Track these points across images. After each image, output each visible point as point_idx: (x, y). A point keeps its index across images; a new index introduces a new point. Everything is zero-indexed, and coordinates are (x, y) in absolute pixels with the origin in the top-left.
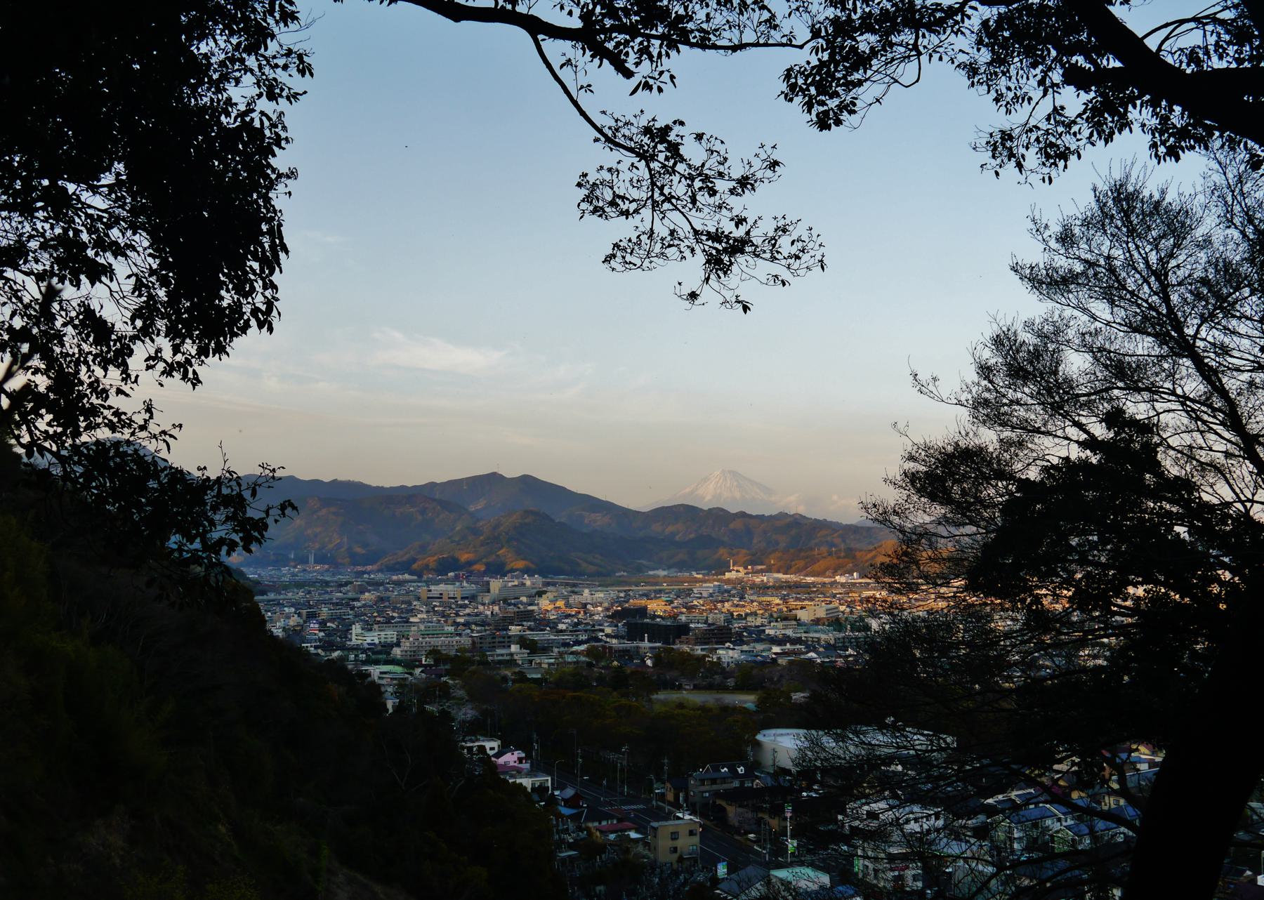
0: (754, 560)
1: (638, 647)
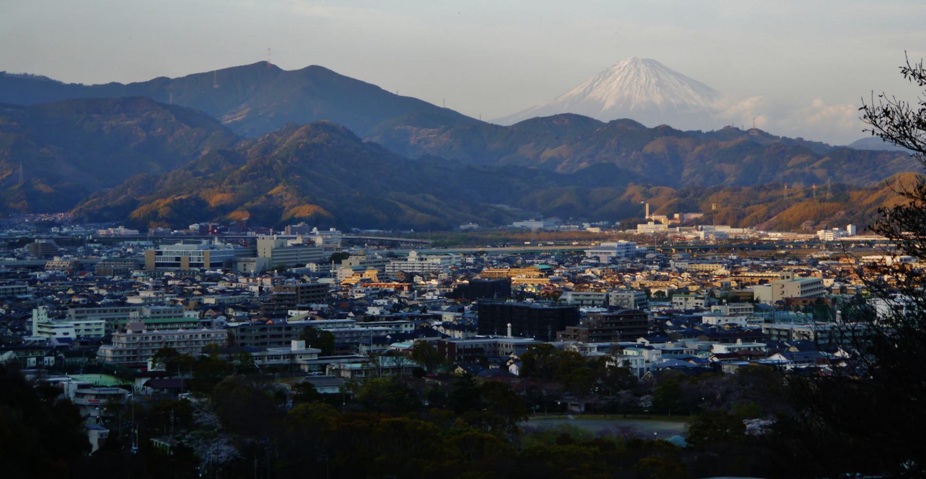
0: (684, 205)
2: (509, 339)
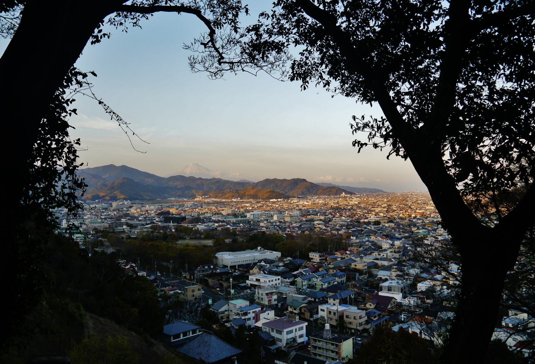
2: (171, 224)
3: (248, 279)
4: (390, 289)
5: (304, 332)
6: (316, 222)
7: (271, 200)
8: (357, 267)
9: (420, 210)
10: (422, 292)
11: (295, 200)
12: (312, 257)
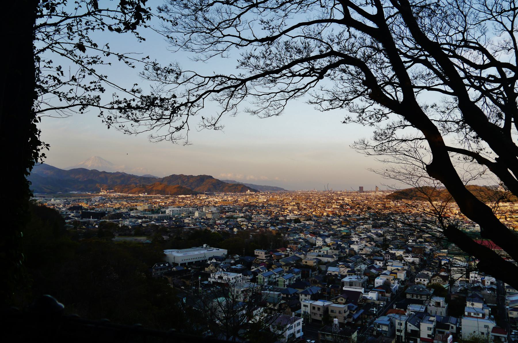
0: (109, 188)
1: (89, 221)
2: (91, 219)
3: (210, 277)
4: (351, 284)
5: (300, 327)
6: (239, 220)
7: (180, 196)
8: (308, 264)
9: (328, 208)
10: (380, 287)
11: (204, 197)
12: (257, 254)
